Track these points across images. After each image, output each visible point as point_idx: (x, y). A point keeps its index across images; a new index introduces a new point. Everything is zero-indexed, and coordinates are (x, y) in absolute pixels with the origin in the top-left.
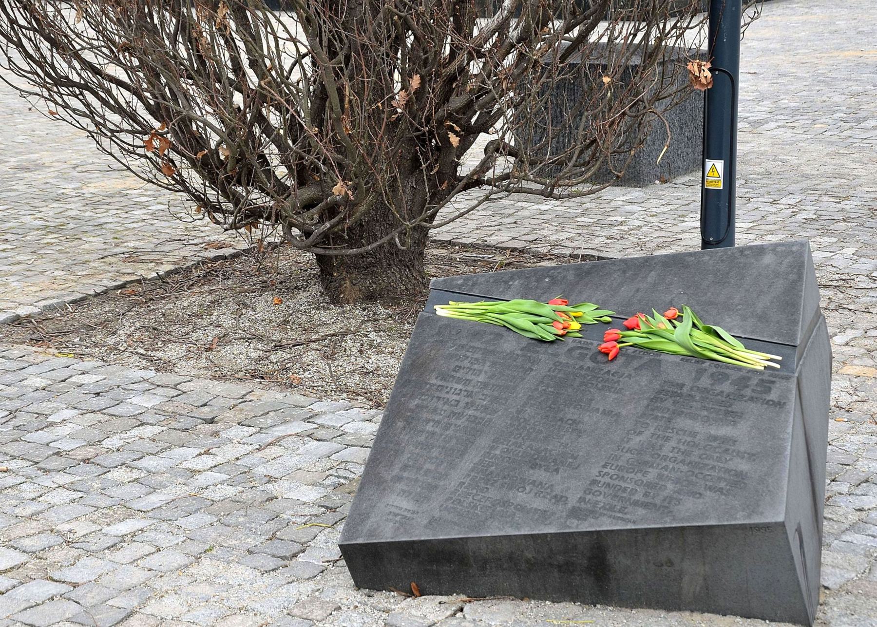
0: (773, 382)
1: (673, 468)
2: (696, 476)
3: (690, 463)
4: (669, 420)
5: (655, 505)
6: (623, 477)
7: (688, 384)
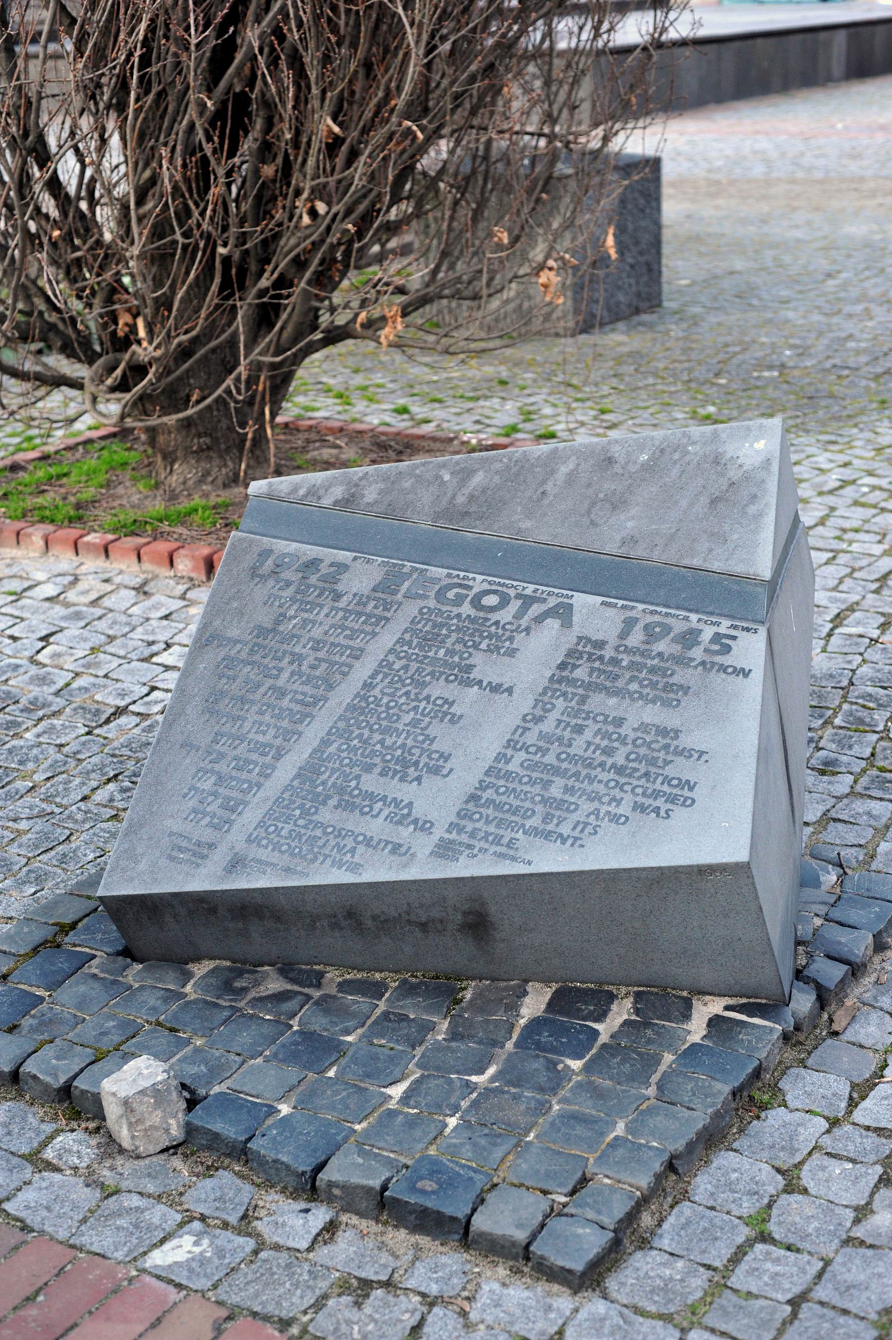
0: (734, 638)
1: (588, 776)
2: (622, 790)
3: (613, 766)
4: (583, 700)
5: (561, 835)
6: (514, 790)
7: (613, 641)
